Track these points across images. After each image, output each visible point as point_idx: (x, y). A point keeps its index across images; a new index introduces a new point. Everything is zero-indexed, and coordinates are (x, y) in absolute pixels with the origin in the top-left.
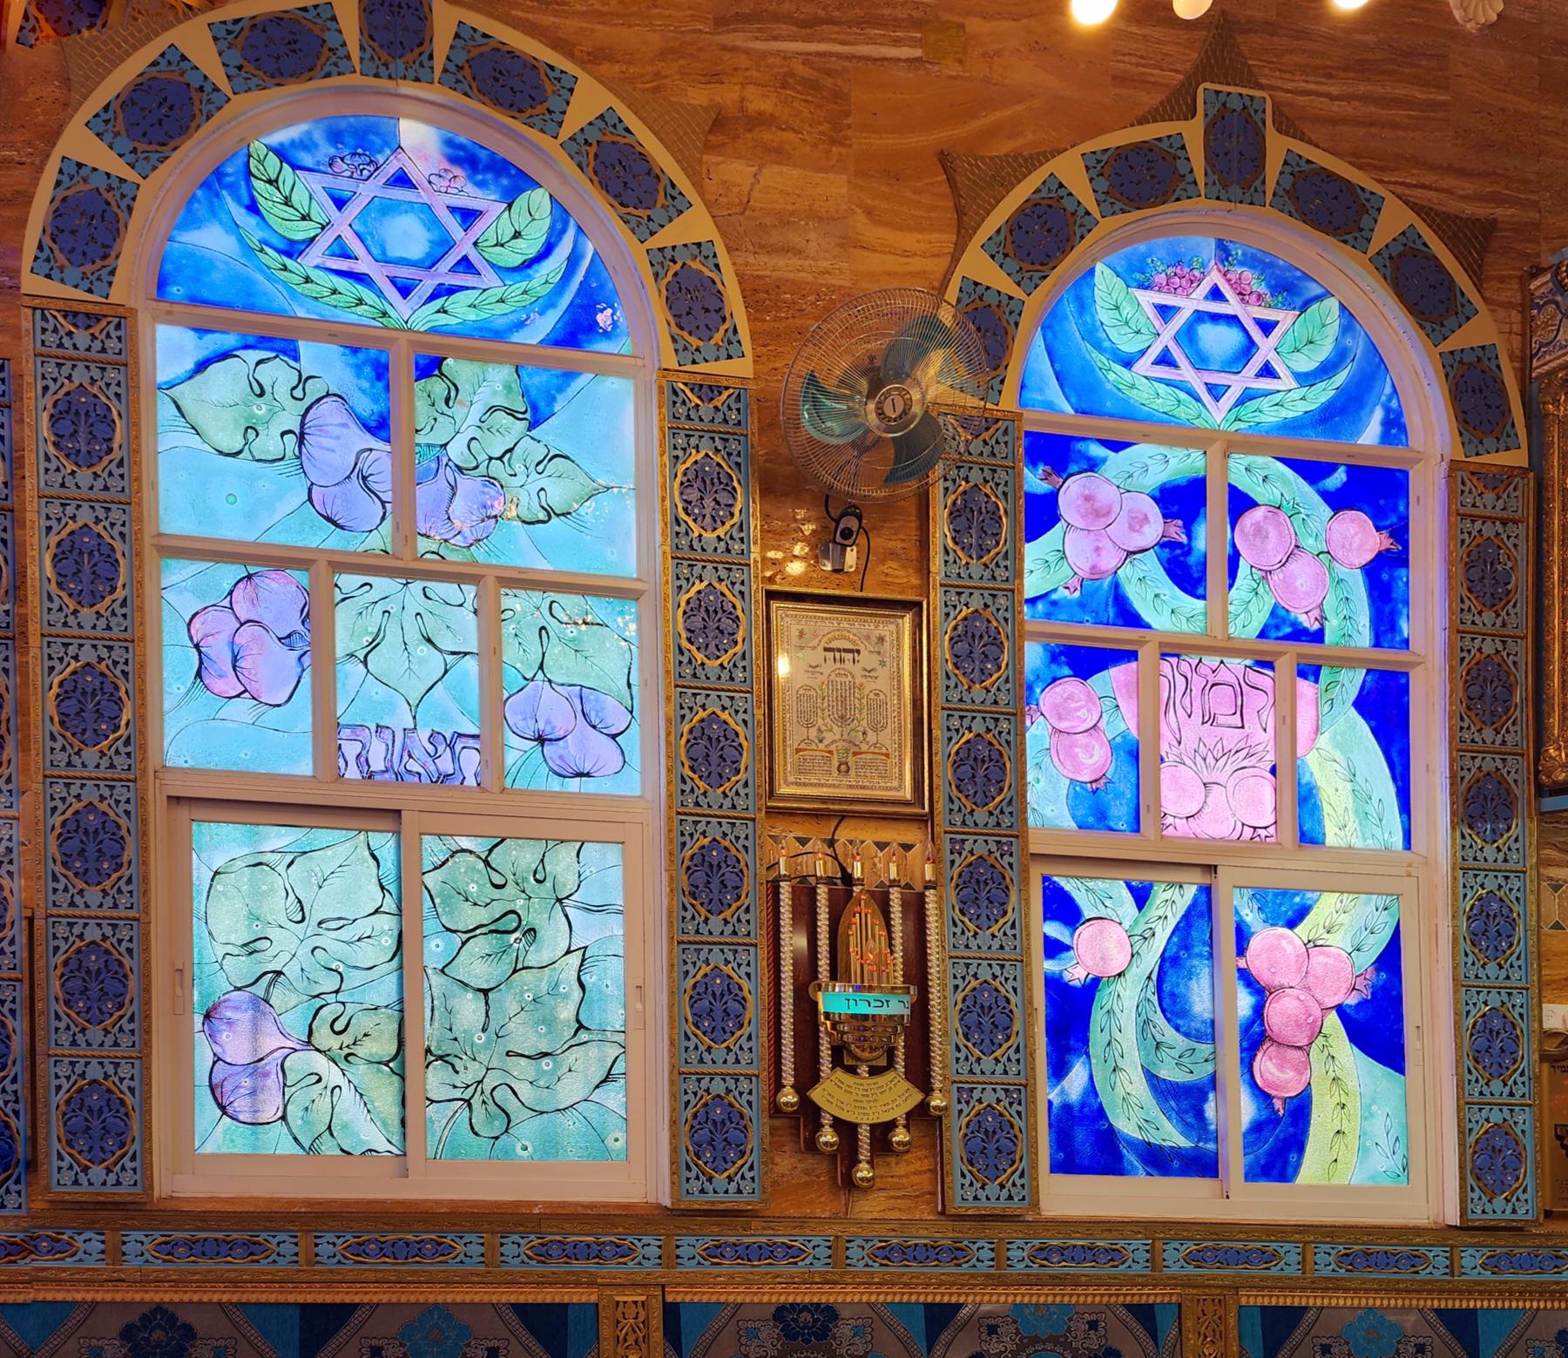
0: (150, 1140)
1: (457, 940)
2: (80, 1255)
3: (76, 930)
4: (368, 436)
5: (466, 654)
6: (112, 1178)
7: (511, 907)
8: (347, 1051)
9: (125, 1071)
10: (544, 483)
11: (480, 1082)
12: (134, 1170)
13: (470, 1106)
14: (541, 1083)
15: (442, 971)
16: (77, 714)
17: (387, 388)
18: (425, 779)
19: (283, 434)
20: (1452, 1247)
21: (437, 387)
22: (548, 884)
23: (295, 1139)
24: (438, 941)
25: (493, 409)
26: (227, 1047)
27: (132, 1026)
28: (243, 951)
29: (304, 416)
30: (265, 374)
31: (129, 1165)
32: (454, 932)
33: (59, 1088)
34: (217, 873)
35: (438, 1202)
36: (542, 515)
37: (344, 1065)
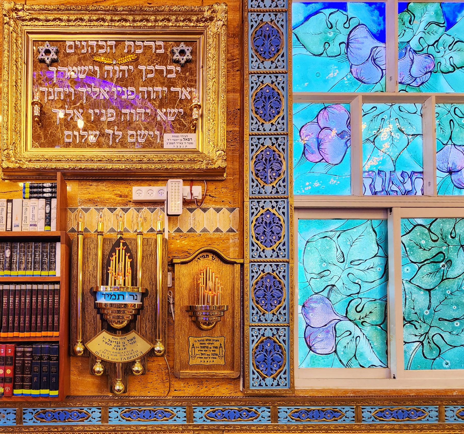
0: (293, 365)
1: (416, 266)
2: (260, 418)
3: (261, 268)
4: (376, 41)
5: (417, 135)
6: (275, 383)
7: (441, 250)
8: (362, 320)
9: (281, 332)
10: (452, 54)
11: (427, 333)
12: (285, 378)
13: (423, 344)
14: (454, 333)
15: (410, 281)
16: (263, 169)
17: (384, 19)
18: (399, 193)
19: (340, 44)
20: (440, 406)
21: (406, 16)
22: (457, 239)
23: (340, 361)
24: (408, 268)
25: (430, 24)
26: (312, 320)
27: (284, 311)
28: (319, 277)
29: (349, 35)
30: (333, 19)
31: (283, 376)
32: (415, 263)
33: (253, 341)
34: (308, 242)
35: (411, 390)
36: (451, 69)
37: (361, 326)
